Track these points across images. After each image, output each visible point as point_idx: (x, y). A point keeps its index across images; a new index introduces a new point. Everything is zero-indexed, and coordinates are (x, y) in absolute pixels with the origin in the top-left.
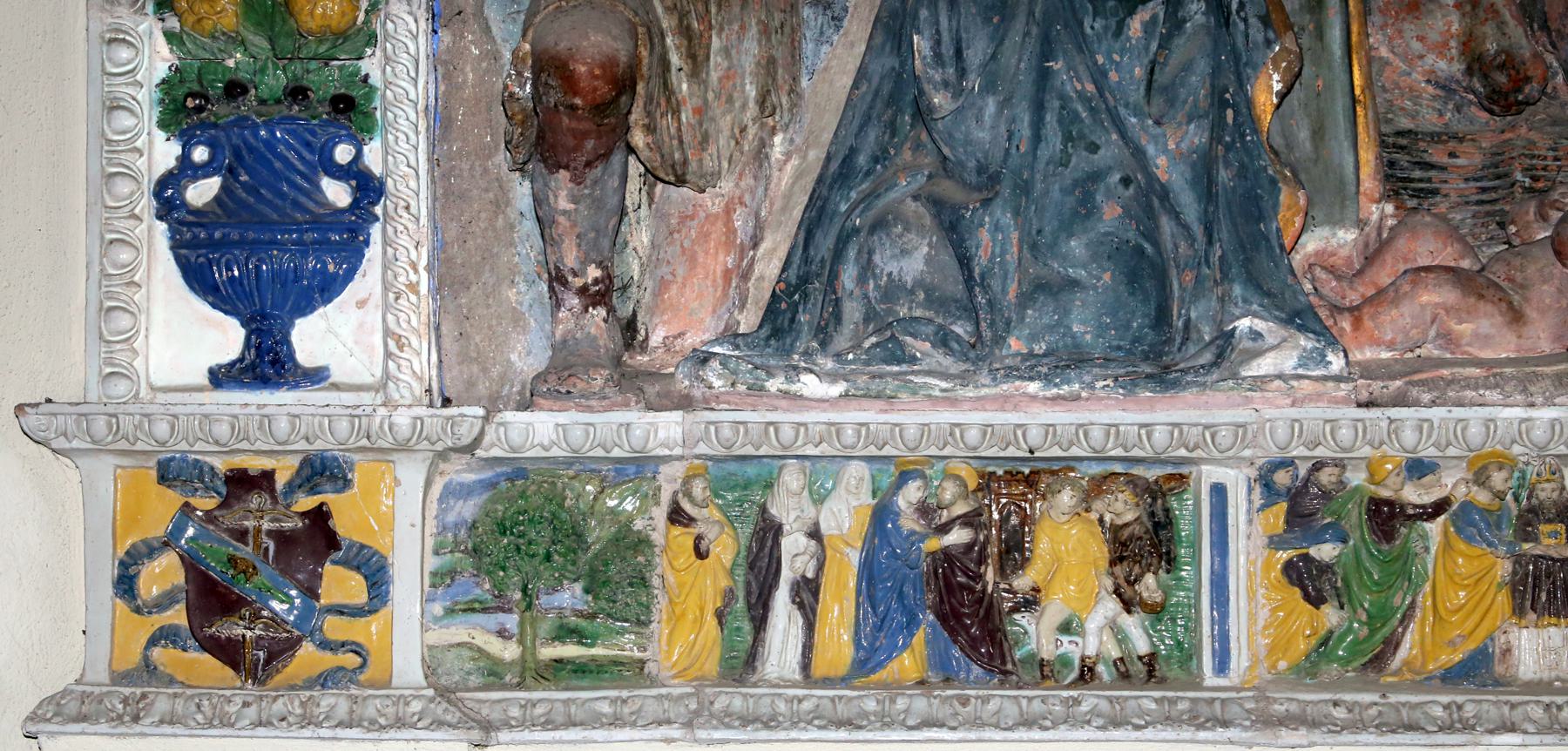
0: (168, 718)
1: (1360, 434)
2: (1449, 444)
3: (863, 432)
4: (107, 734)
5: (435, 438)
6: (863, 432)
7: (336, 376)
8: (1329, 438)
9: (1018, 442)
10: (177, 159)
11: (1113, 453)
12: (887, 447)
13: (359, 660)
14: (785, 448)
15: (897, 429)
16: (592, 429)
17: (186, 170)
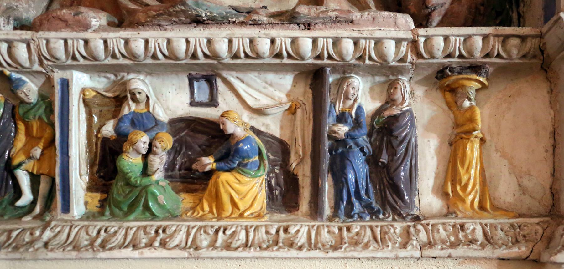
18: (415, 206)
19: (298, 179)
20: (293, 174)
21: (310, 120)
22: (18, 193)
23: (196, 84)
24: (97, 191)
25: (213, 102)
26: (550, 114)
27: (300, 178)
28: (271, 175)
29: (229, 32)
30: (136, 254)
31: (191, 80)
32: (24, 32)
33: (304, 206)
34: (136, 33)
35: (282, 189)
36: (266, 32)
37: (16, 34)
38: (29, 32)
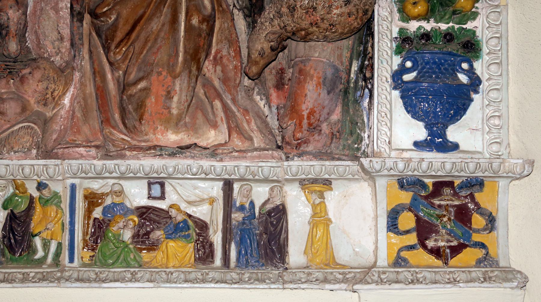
0: (149, 280)
1: (33, 172)
2: (486, 171)
3: (248, 170)
4: (45, 287)
5: (207, 173)
6: (248, 170)
7: (462, 147)
8: (45, 172)
9: (188, 172)
10: (398, 65)
11: (249, 177)
12: (162, 174)
13: (484, 251)
14: (169, 175)
15: (260, 169)
16: (300, 167)
17: (402, 70)
18: (285, 262)
19: (472, 100)
20: (211, 242)
21: (221, 209)
22: (35, 252)
23: (152, 186)
24: (431, 248)
25: (162, 197)
26: (372, 207)
27: (215, 244)
28: (198, 242)
29: (176, 162)
30: (123, 285)
31: (150, 184)
32: (56, 160)
33: (218, 261)
34: (123, 161)
35: (11, 98)
36: (198, 162)
37: (52, 162)
38: (59, 160)
